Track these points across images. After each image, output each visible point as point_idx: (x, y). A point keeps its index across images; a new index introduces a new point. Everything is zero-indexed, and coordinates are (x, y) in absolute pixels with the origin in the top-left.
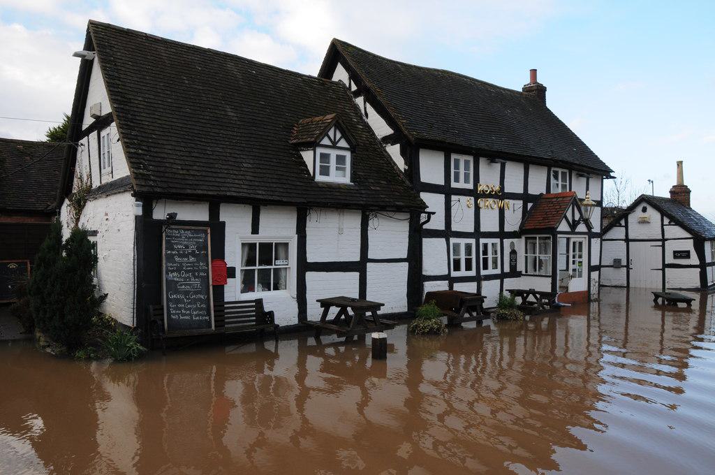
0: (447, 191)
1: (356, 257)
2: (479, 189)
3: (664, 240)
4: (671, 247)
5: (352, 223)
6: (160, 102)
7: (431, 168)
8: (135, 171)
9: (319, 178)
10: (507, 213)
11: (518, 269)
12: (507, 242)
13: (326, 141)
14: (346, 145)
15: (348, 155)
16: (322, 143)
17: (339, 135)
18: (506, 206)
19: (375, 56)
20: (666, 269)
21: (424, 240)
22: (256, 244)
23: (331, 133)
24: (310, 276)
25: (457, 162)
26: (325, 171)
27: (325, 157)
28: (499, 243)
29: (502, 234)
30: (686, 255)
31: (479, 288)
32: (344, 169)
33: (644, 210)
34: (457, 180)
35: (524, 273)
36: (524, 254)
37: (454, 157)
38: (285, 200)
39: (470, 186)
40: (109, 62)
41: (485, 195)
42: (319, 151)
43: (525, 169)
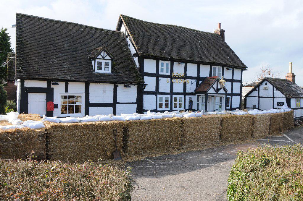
0: (157, 76)
1: (111, 102)
2: (173, 75)
3: (274, 97)
4: (277, 100)
5: (110, 88)
7: (150, 66)
10: (187, 85)
11: (193, 108)
12: (187, 97)
13: (100, 57)
14: (109, 58)
15: (110, 62)
16: (98, 58)
17: (106, 54)
18: (187, 82)
19: (138, 21)
21: (233, 93)
22: (67, 96)
23: (102, 54)
25: (162, 64)
26: (100, 68)
27: (100, 63)
29: (185, 94)
30: (283, 104)
32: (108, 68)
33: (266, 84)
35: (196, 110)
36: (196, 102)
37: (161, 62)
38: (77, 80)
39: (169, 74)
40: (20, 29)
41: (176, 77)
42: (97, 61)
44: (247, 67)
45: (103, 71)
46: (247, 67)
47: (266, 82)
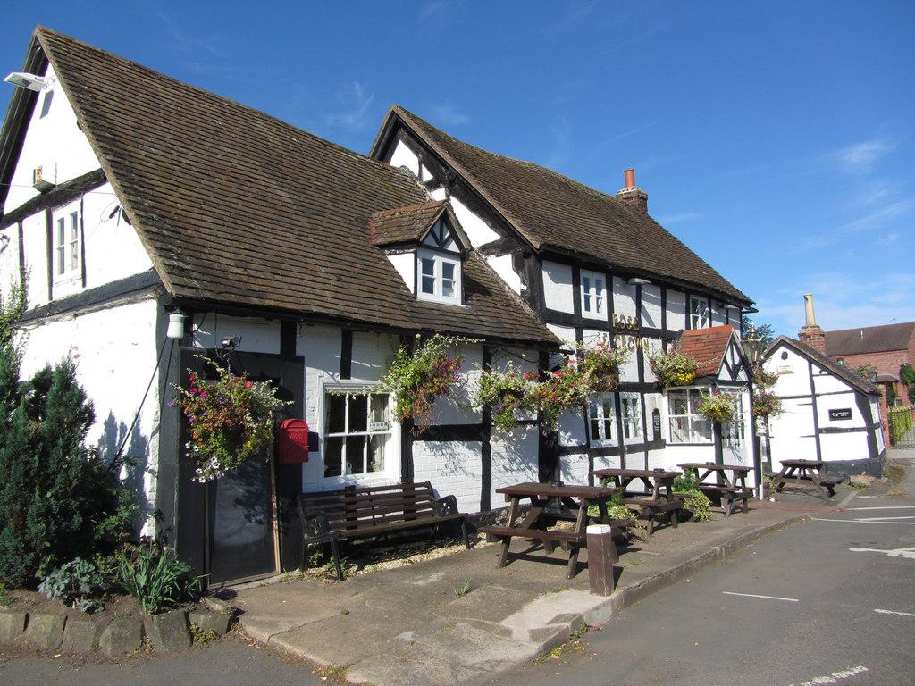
3: (814, 396)
4: (825, 405)
6: (174, 162)
8: (166, 262)
9: (423, 296)
20: (820, 435)
22: (343, 397)
24: (419, 448)
26: (428, 287)
28: (613, 400)
30: (847, 414)
31: (623, 464)
33: (785, 356)
34: (588, 308)
43: (662, 293)
44: (752, 303)
45: (437, 297)
46: (752, 303)
47: (782, 349)
